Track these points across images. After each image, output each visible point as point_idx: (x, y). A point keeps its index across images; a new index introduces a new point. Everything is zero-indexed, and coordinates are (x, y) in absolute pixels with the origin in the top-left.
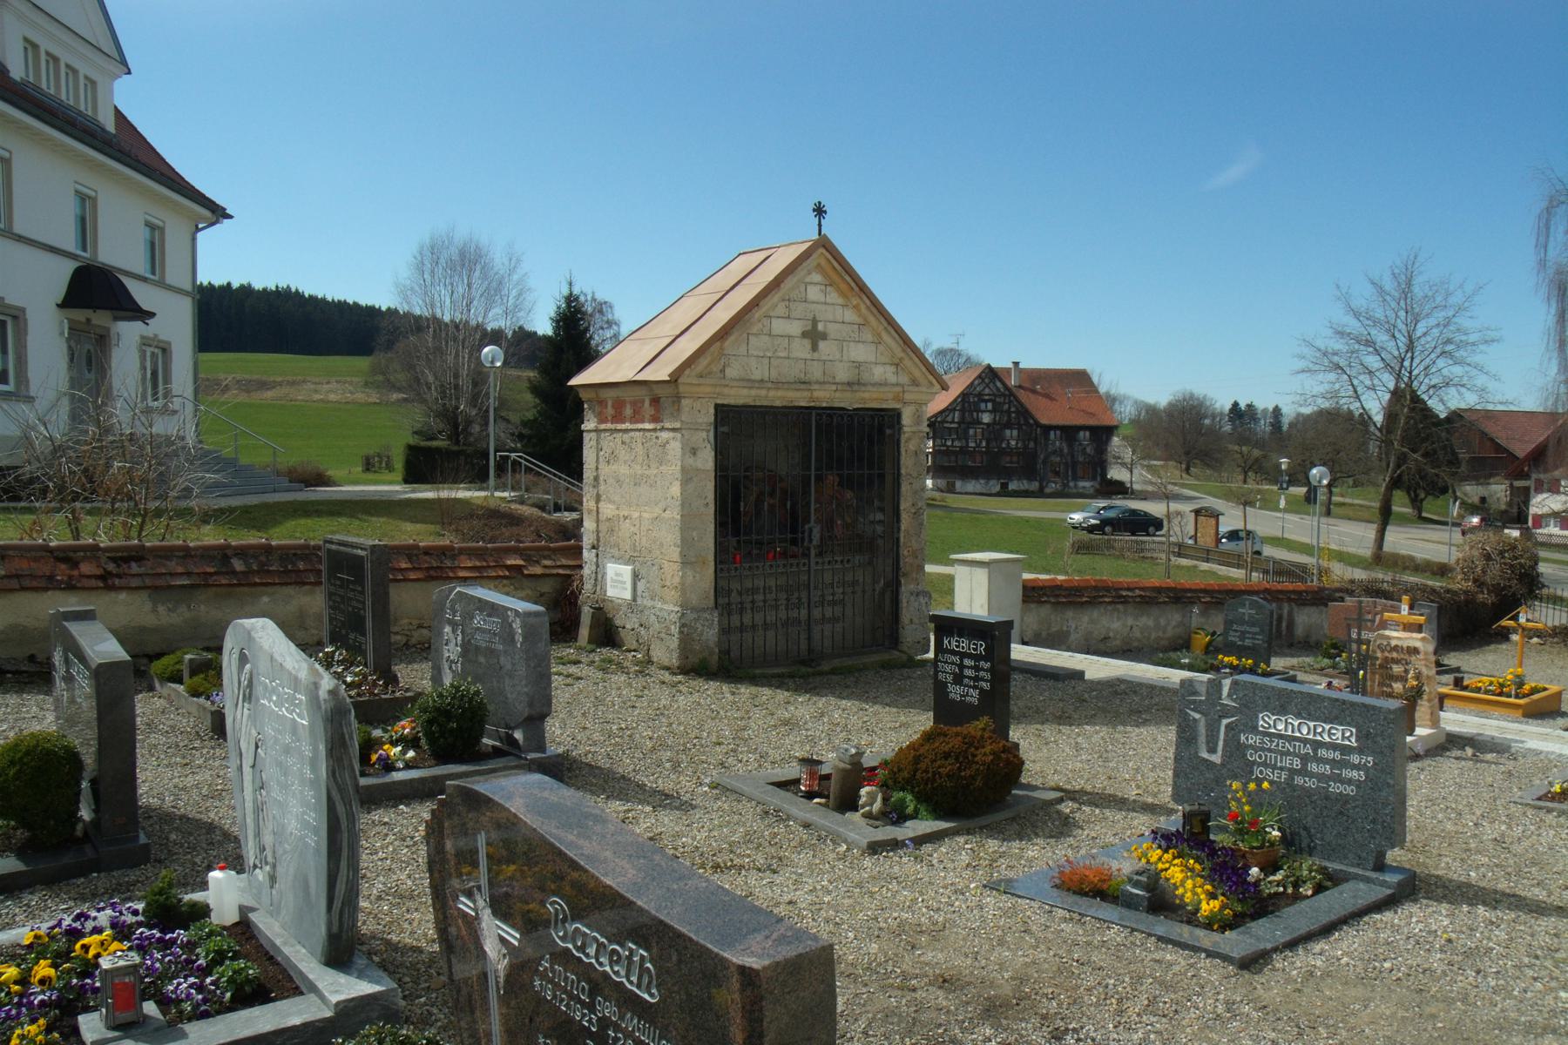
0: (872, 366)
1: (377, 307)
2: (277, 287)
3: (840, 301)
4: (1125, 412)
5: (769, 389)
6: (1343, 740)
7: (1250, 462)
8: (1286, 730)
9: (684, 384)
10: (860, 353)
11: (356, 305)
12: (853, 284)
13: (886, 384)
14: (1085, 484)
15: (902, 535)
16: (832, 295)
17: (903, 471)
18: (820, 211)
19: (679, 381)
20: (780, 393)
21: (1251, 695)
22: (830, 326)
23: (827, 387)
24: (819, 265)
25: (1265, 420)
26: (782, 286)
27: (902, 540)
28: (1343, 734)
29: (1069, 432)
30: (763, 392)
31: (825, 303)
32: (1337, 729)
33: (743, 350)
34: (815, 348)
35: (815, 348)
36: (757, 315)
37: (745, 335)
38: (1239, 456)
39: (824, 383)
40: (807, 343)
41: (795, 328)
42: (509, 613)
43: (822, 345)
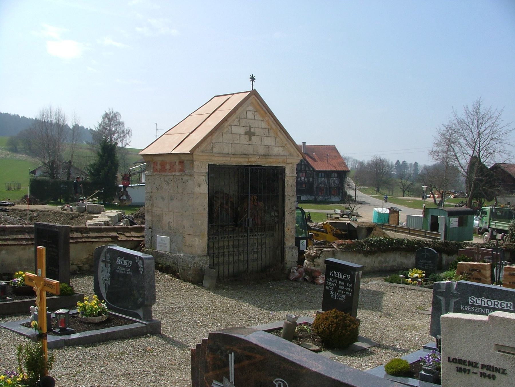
0: (274, 147)
1: (9, 113)
2: (304, 143)
3: (261, 118)
4: (350, 166)
5: (231, 157)
6: (507, 308)
7: (405, 188)
8: (481, 304)
9: (195, 155)
10: (269, 141)
11: (24, 118)
12: (266, 111)
13: (279, 156)
14: (336, 199)
15: (285, 222)
16: (257, 116)
17: (286, 194)
18: (252, 79)
19: (194, 153)
20: (235, 159)
21: (466, 289)
22: (257, 130)
23: (255, 156)
24: (252, 102)
25: (411, 168)
26: (237, 111)
27: (285, 224)
28: (507, 305)
29: (328, 174)
30: (229, 159)
31: (254, 119)
32: (504, 303)
33: (220, 140)
34: (250, 139)
35: (250, 139)
36: (226, 125)
37: (221, 134)
38: (401, 184)
39: (254, 155)
40: (247, 137)
41: (242, 130)
42: (136, 258)
43: (253, 138)
